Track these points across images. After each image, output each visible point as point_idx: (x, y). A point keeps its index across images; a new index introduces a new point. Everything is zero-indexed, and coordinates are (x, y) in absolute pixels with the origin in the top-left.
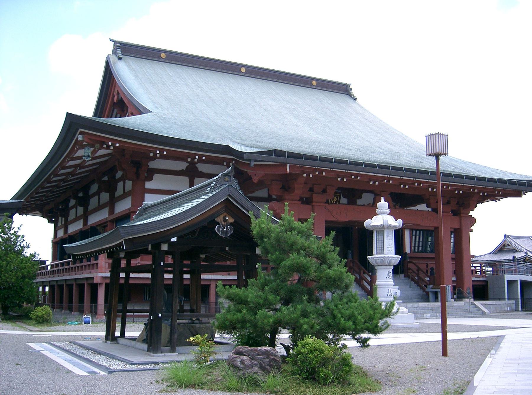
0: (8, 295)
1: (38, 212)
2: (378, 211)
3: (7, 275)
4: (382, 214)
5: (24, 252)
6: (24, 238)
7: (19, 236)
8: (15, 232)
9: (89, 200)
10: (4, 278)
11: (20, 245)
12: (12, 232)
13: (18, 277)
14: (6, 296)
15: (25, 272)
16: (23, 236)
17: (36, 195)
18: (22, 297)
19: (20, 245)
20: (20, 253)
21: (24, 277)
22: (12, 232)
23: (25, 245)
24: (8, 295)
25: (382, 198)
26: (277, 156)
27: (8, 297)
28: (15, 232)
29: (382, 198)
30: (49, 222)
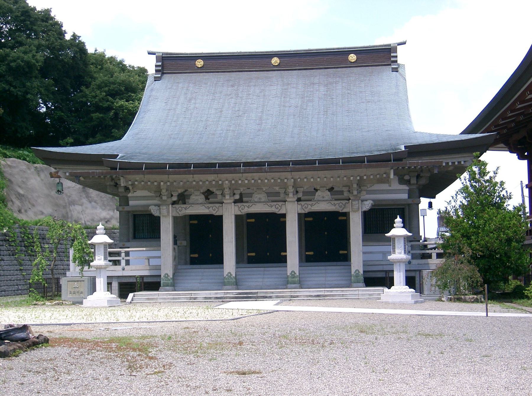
0: (490, 266)
1: (502, 145)
2: (395, 225)
3: (487, 239)
4: (398, 227)
5: (505, 205)
6: (505, 186)
7: (497, 183)
8: (491, 178)
9: (487, 149)
10: (483, 242)
11: (499, 196)
12: (487, 178)
13: (501, 241)
14: (487, 267)
15: (510, 233)
16: (502, 183)
17: (510, 115)
18: (509, 267)
19: (499, 196)
20: (499, 206)
21: (509, 241)
22: (487, 178)
23: (505, 195)
24: (490, 266)
25: (398, 216)
26: (341, 191)
27: (490, 268)
28: (491, 178)
29: (398, 216)
30: (519, 158)
